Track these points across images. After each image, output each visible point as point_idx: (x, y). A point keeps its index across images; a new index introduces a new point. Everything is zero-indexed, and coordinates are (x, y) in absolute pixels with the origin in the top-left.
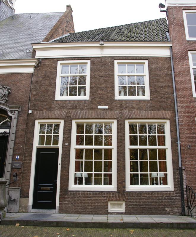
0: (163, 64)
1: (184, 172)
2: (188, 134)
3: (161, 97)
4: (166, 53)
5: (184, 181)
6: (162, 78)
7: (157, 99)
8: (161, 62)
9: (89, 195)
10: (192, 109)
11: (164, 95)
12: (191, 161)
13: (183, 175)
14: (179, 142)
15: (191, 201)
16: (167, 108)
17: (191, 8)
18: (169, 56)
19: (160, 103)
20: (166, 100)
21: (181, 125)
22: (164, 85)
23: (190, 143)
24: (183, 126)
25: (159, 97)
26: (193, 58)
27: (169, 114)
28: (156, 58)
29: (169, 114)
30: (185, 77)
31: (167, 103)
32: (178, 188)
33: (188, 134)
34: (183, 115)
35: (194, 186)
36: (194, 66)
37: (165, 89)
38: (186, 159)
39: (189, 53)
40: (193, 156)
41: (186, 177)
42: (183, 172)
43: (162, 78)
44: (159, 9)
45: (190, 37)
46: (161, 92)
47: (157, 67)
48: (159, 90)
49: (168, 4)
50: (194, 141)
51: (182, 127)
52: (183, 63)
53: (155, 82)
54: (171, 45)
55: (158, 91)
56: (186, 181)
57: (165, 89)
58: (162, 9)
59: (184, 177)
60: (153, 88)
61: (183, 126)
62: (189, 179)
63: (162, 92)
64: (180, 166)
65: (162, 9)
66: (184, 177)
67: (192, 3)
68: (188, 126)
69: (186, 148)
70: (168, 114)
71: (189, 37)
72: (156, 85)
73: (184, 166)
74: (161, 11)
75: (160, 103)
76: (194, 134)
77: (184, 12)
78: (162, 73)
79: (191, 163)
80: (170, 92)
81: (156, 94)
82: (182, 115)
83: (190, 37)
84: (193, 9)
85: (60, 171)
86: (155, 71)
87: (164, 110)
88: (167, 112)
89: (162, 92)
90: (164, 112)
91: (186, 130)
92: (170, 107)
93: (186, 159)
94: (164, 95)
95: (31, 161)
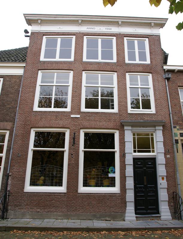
0: (15, 82)
1: (10, 178)
2: (21, 143)
3: (7, 111)
4: (20, 72)
5: (9, 186)
6: (11, 93)
7: (3, 112)
8: (14, 80)
9: (105, 197)
10: (29, 121)
11: (10, 108)
12: (18, 168)
13: (9, 180)
14: (11, 151)
15: (177, 202)
16: (10, 120)
17: (54, 34)
18: (22, 75)
19: (5, 115)
20: (11, 113)
21: (16, 135)
22: (11, 100)
23: (21, 151)
24: (17, 136)
25: (5, 111)
26: (101, 79)
27: (10, 125)
28: (11, 76)
29: (10, 125)
30: (29, 92)
31: (10, 115)
32: (3, 193)
33: (21, 143)
34: (20, 127)
35: (17, 191)
36: (86, 84)
37: (12, 103)
38: (14, 166)
39: (127, 74)
40: (21, 163)
41: (11, 183)
42: (9, 178)
43: (11, 93)
44: (24, 34)
45: (129, 60)
46: (7, 106)
47: (9, 84)
48: (6, 104)
49: (31, 30)
50: (25, 150)
51: (17, 137)
52: (31, 81)
53: (4, 97)
54: (25, 65)
55: (5, 105)
56: (11, 186)
57: (12, 103)
58: (27, 34)
59: (10, 182)
60: (2, 102)
61: (17, 136)
62: (13, 184)
63: (9, 106)
64: (8, 172)
65: (27, 34)
66: (9, 183)
67: (55, 30)
68: (22, 137)
69: (16, 156)
70: (9, 125)
71: (129, 60)
72: (4, 100)
73: (11, 172)
74: (26, 36)
75: (5, 115)
76: (26, 143)
77: (125, 38)
78: (13, 90)
79: (17, 170)
80: (15, 106)
81: (3, 108)
82: (18, 127)
83: (129, 60)
84: (52, 35)
85: (2, 178)
86: (7, 88)
87: (7, 122)
88: (9, 124)
89: (9, 106)
90: (6, 123)
91: (20, 140)
92: (12, 119)
93: (14, 166)
94: (10, 109)
95: (78, 168)
